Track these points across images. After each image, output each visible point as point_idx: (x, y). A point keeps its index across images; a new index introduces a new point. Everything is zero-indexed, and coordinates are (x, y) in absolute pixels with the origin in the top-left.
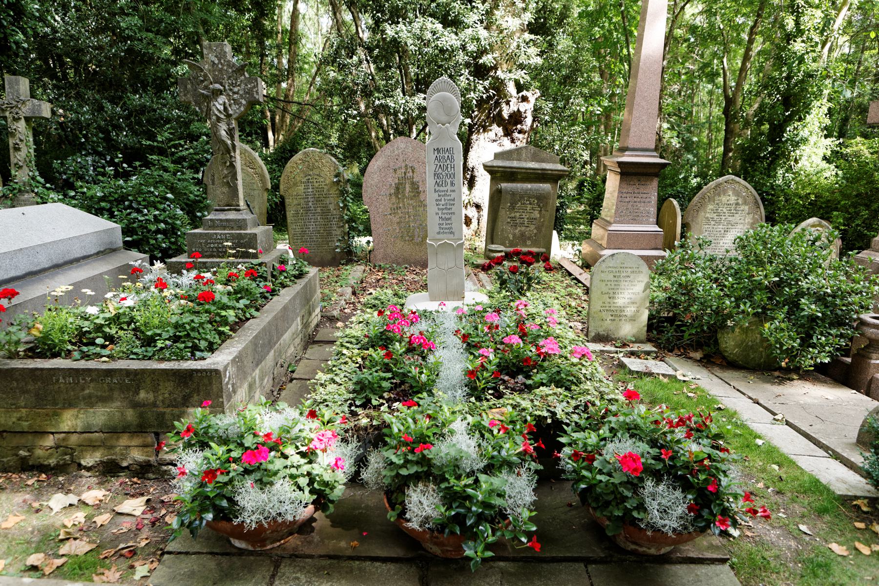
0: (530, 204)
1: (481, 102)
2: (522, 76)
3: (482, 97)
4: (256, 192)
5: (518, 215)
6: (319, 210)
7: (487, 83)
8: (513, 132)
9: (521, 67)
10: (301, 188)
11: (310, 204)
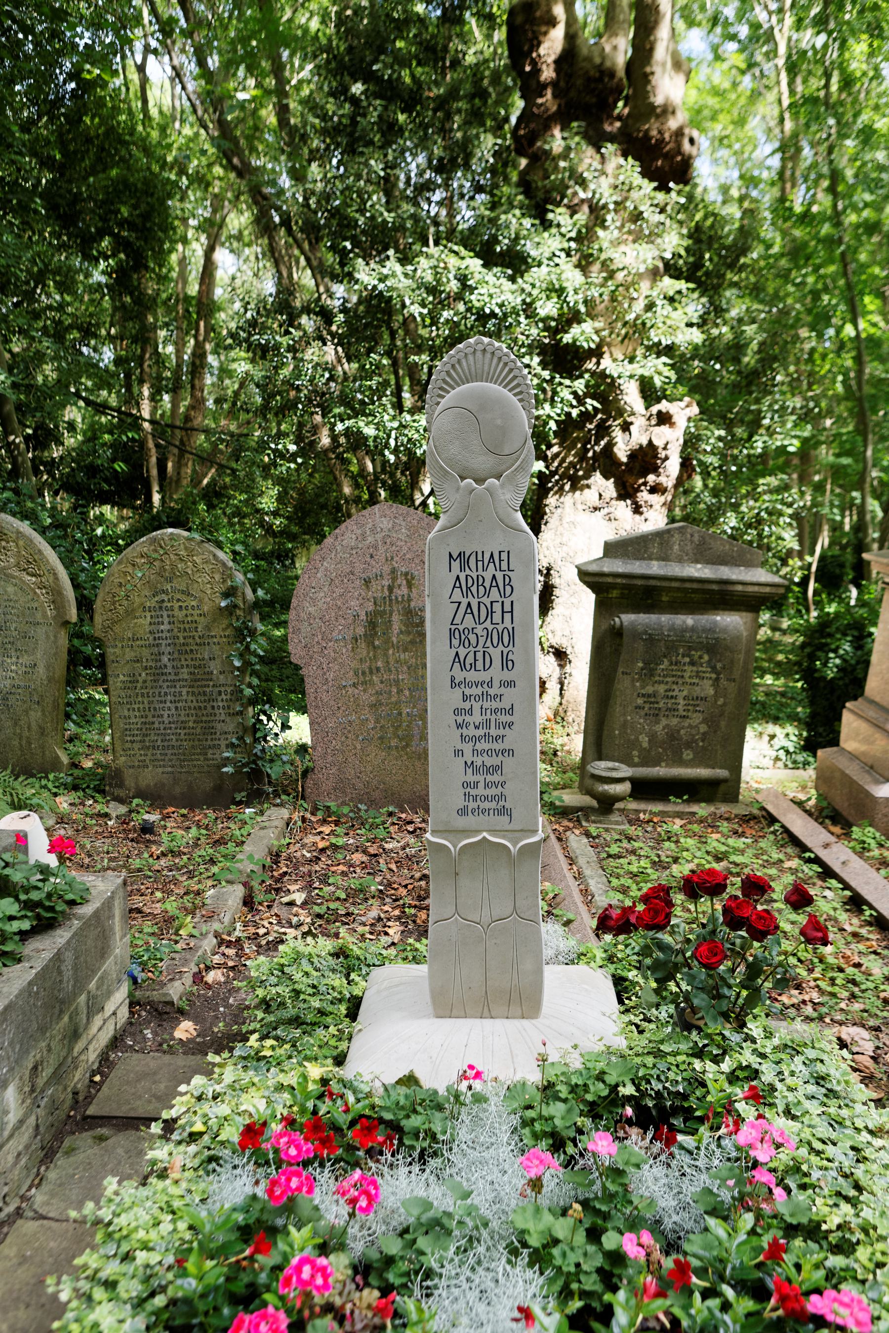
0: (692, 663)
1: (567, 426)
2: (658, 369)
3: (568, 414)
4: (41, 631)
5: (661, 689)
6: (184, 674)
7: (579, 385)
8: (638, 490)
9: (659, 350)
10: (144, 621)
11: (165, 659)
